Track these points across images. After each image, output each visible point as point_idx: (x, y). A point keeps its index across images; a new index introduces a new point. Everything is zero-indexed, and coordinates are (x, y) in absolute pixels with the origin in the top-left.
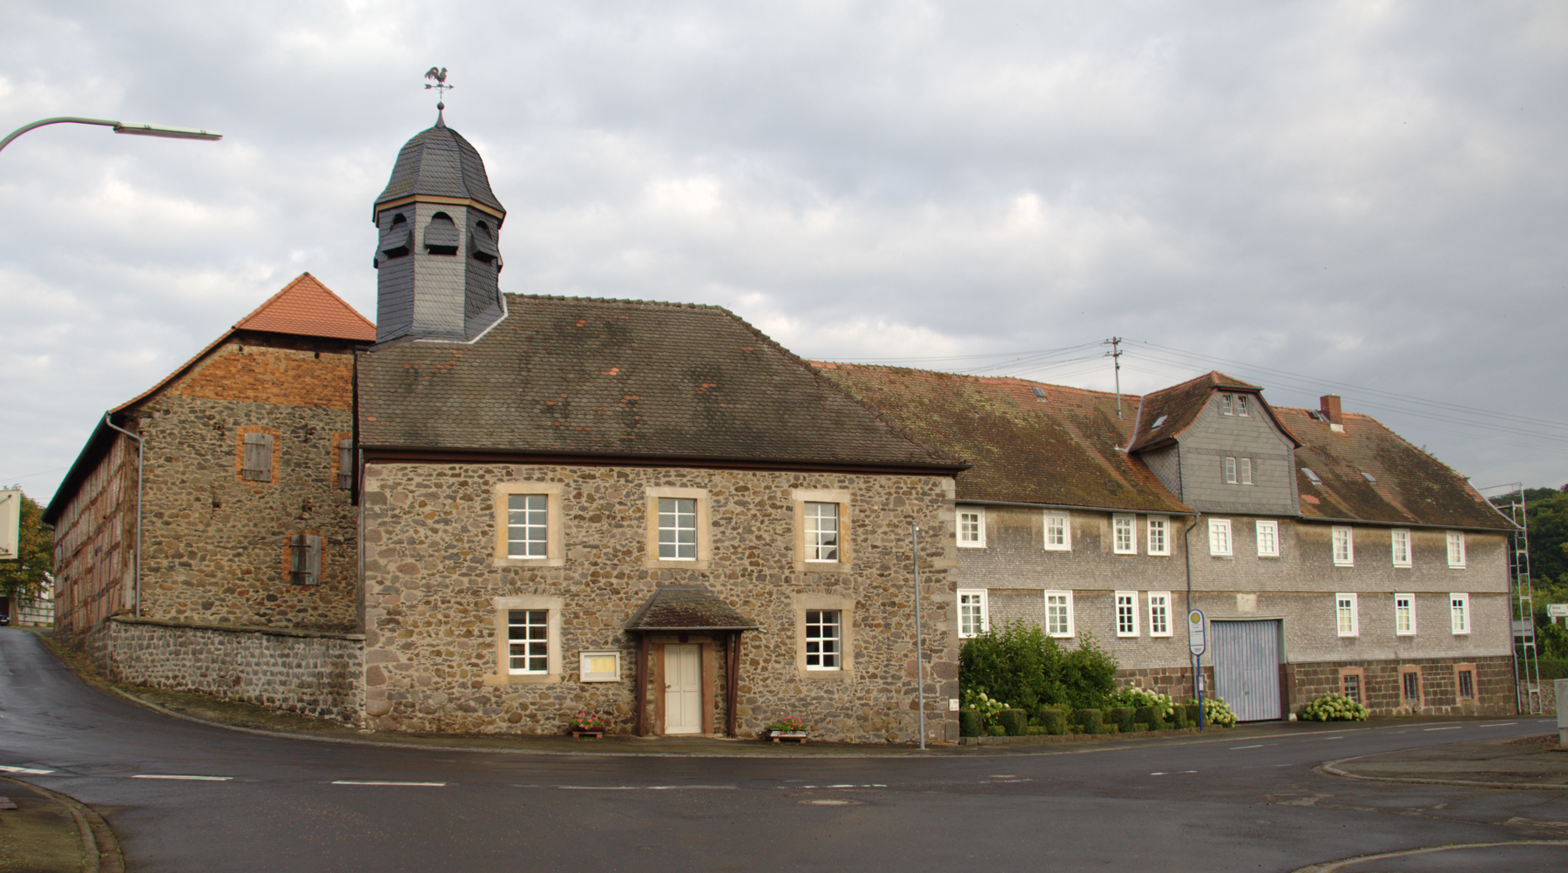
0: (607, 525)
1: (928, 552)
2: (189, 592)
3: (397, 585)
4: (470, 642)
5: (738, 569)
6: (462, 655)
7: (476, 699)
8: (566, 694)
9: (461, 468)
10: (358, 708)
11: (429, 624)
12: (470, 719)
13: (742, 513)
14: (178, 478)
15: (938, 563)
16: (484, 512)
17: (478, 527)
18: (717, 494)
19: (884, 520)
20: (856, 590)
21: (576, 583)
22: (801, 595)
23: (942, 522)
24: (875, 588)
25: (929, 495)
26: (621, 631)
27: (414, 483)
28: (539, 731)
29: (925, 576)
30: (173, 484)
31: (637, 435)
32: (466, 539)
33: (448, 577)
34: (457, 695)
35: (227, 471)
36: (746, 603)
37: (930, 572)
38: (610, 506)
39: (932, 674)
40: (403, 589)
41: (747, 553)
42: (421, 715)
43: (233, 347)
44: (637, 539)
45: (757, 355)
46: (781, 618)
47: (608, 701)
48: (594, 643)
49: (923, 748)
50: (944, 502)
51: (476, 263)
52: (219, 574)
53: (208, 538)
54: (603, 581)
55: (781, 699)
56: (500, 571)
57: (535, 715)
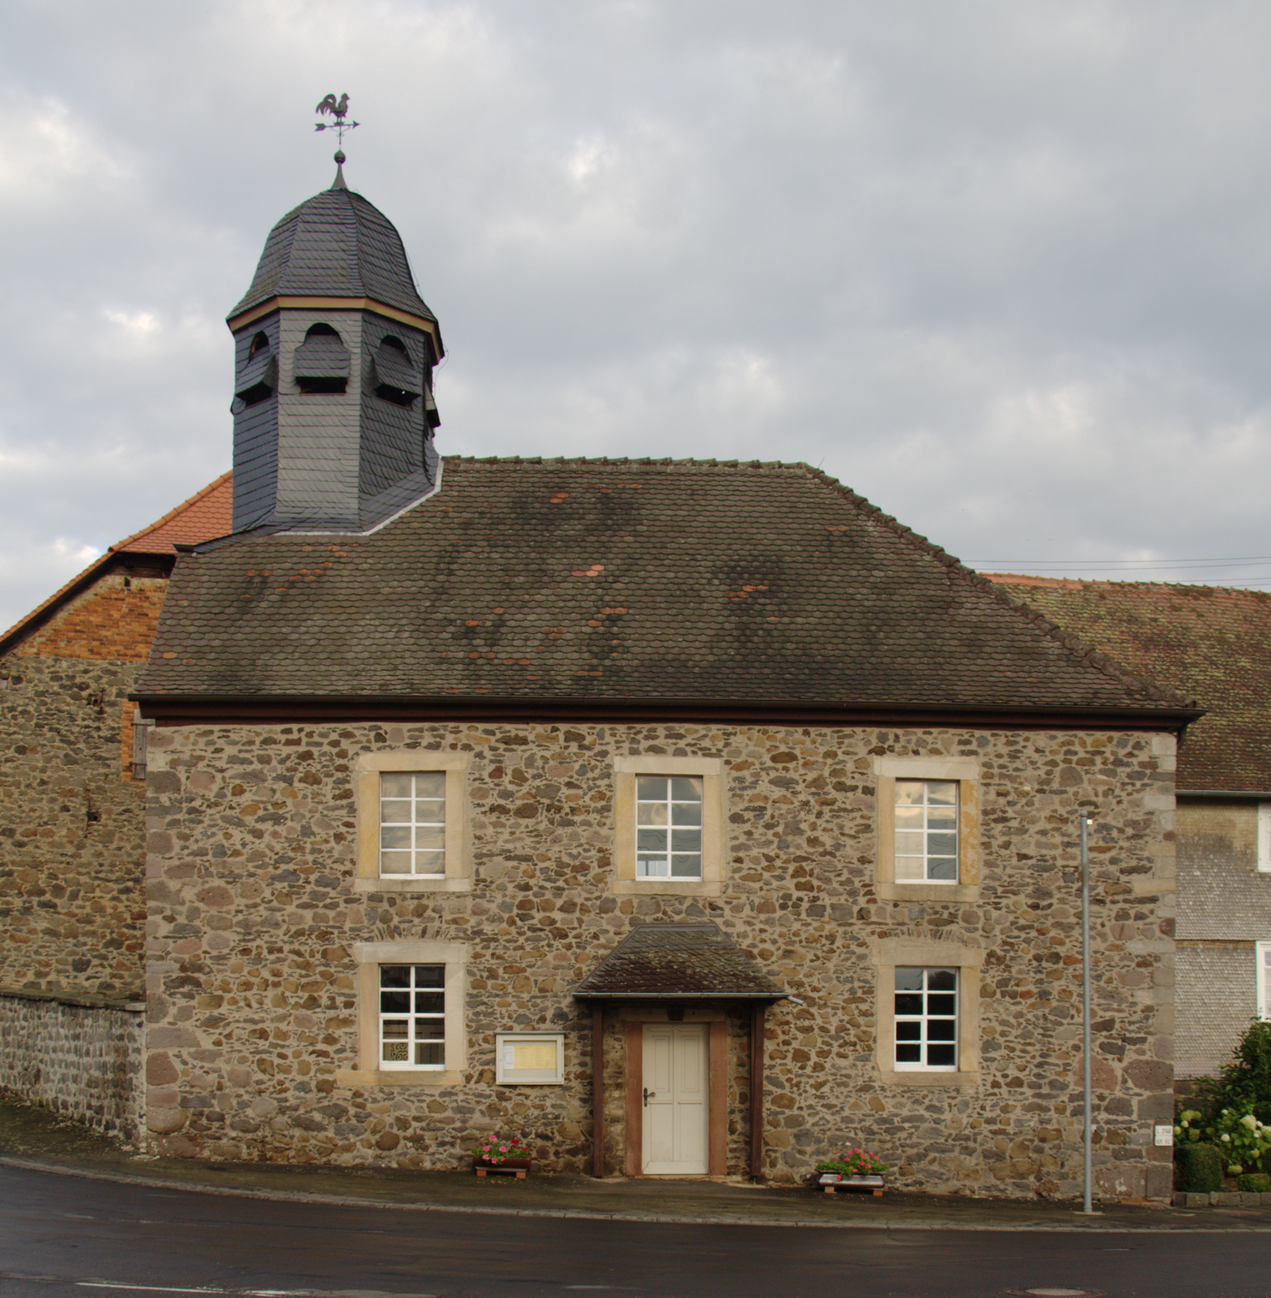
0: (546, 822)
1: (1123, 865)
2: (54, 946)
3: (197, 923)
4: (314, 1016)
5: (775, 895)
6: (301, 1037)
7: (323, 1110)
8: (473, 1105)
9: (300, 730)
11: (247, 986)
12: (313, 1142)
13: (784, 799)
14: (35, 778)
15: (1141, 885)
16: (339, 802)
17: (329, 826)
18: (739, 767)
19: (1042, 809)
20: (987, 933)
21: (492, 920)
22: (886, 940)
23: (1151, 813)
24: (1022, 928)
25: (1128, 765)
26: (569, 1000)
27: (224, 755)
28: (427, 1165)
29: (1116, 908)
30: (29, 786)
31: (607, 669)
32: (308, 846)
33: (280, 910)
34: (292, 1102)
35: (109, 766)
36: (788, 954)
37: (1125, 901)
38: (551, 790)
39: (1125, 1081)
40: (206, 929)
41: (792, 867)
42: (234, 1134)
43: (114, 580)
44: (598, 845)
45: (851, 539)
46: (850, 980)
47: (545, 1116)
48: (521, 1019)
49: (1089, 1210)
50: (1156, 776)
51: (382, 405)
52: (99, 919)
53: (81, 865)
54: (538, 916)
55: (847, 1120)
56: (364, 899)
57: (421, 1138)
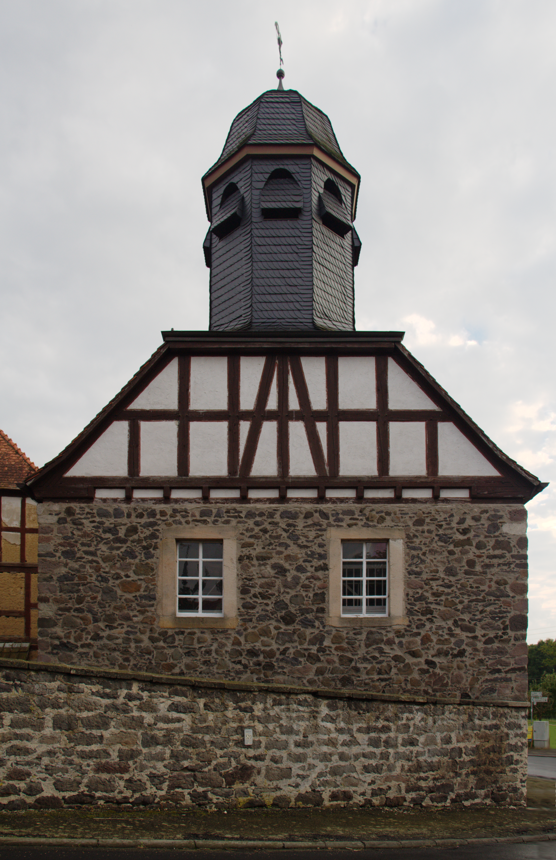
10: (519, 784)
